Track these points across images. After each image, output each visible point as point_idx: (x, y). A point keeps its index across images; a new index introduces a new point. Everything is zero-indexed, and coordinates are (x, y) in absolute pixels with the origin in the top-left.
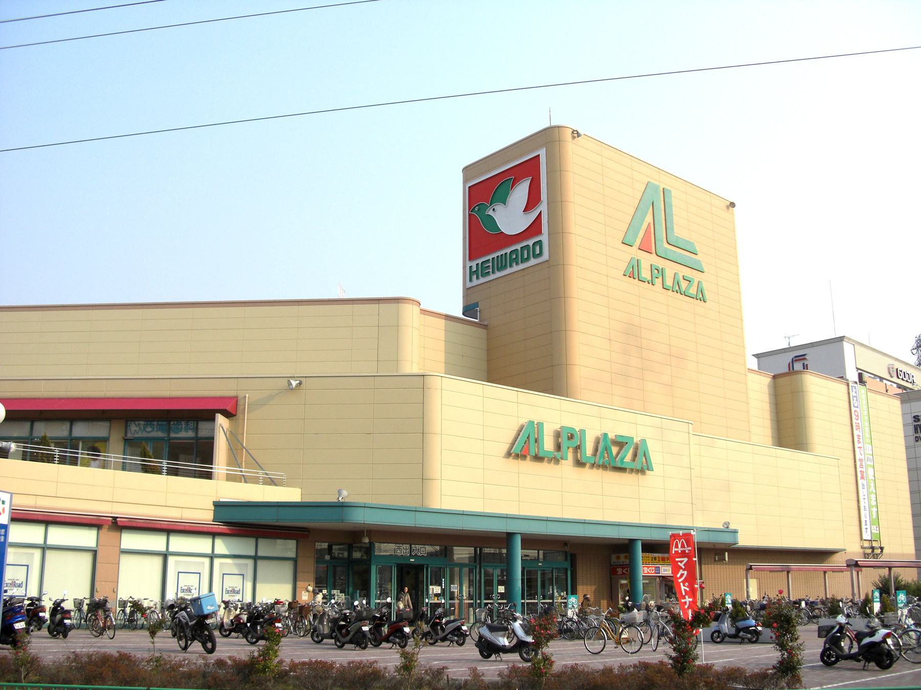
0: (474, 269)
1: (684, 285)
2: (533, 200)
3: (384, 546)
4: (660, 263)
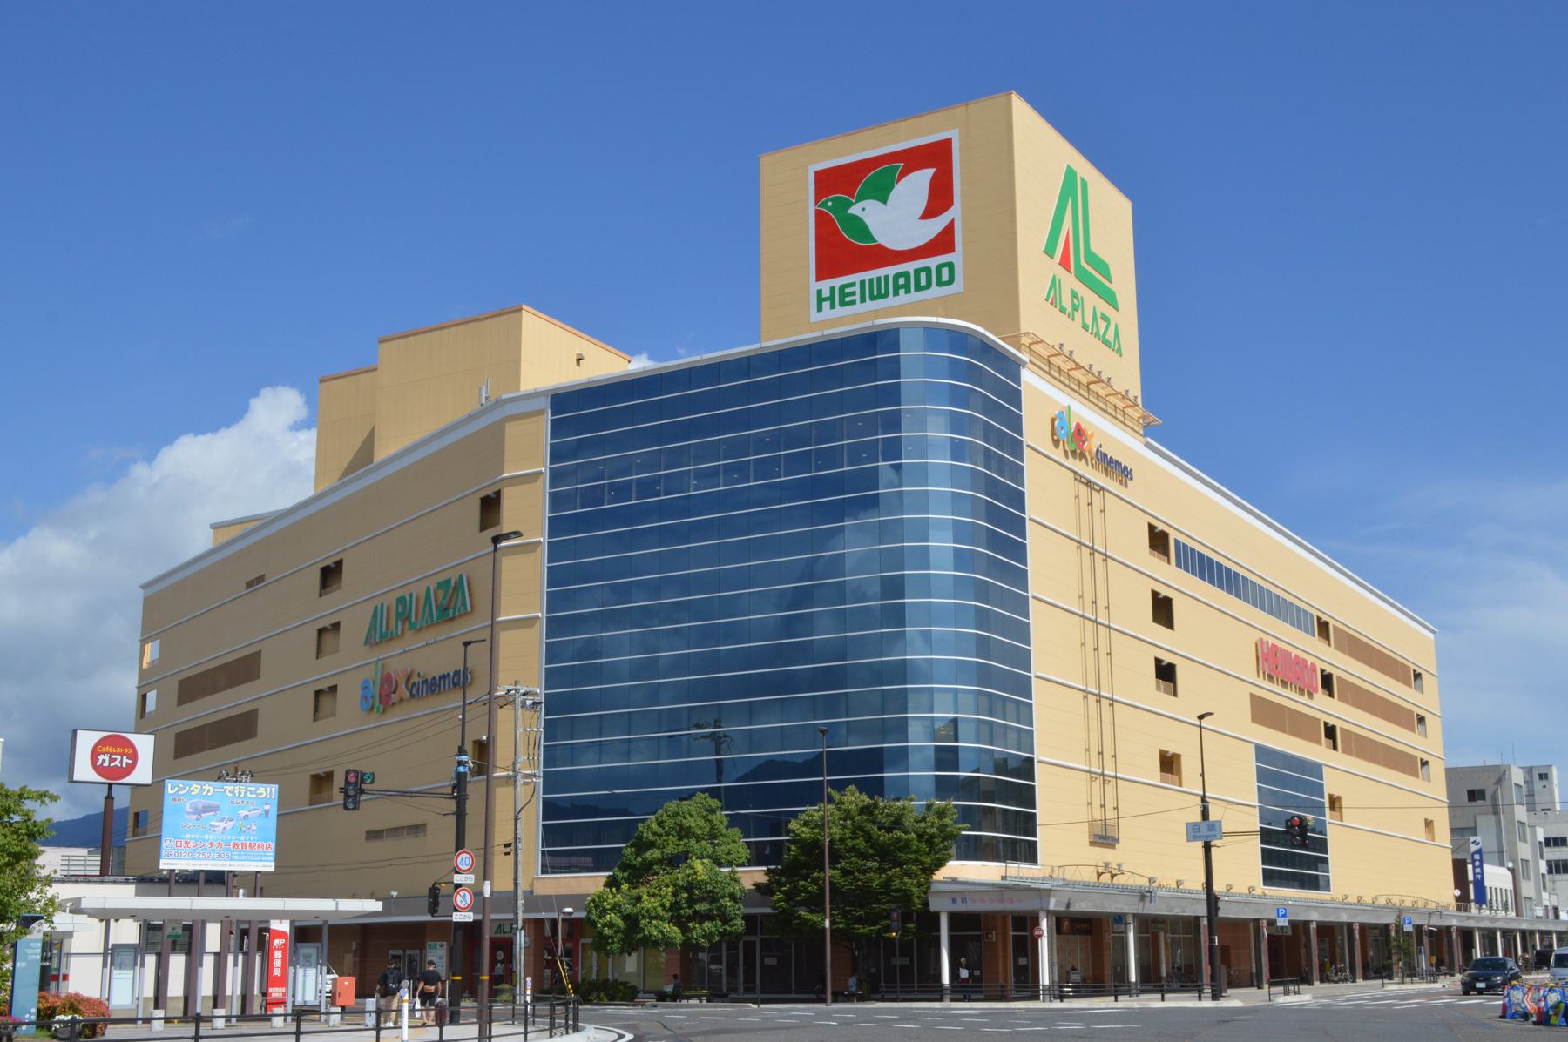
0: (826, 294)
1: (1103, 325)
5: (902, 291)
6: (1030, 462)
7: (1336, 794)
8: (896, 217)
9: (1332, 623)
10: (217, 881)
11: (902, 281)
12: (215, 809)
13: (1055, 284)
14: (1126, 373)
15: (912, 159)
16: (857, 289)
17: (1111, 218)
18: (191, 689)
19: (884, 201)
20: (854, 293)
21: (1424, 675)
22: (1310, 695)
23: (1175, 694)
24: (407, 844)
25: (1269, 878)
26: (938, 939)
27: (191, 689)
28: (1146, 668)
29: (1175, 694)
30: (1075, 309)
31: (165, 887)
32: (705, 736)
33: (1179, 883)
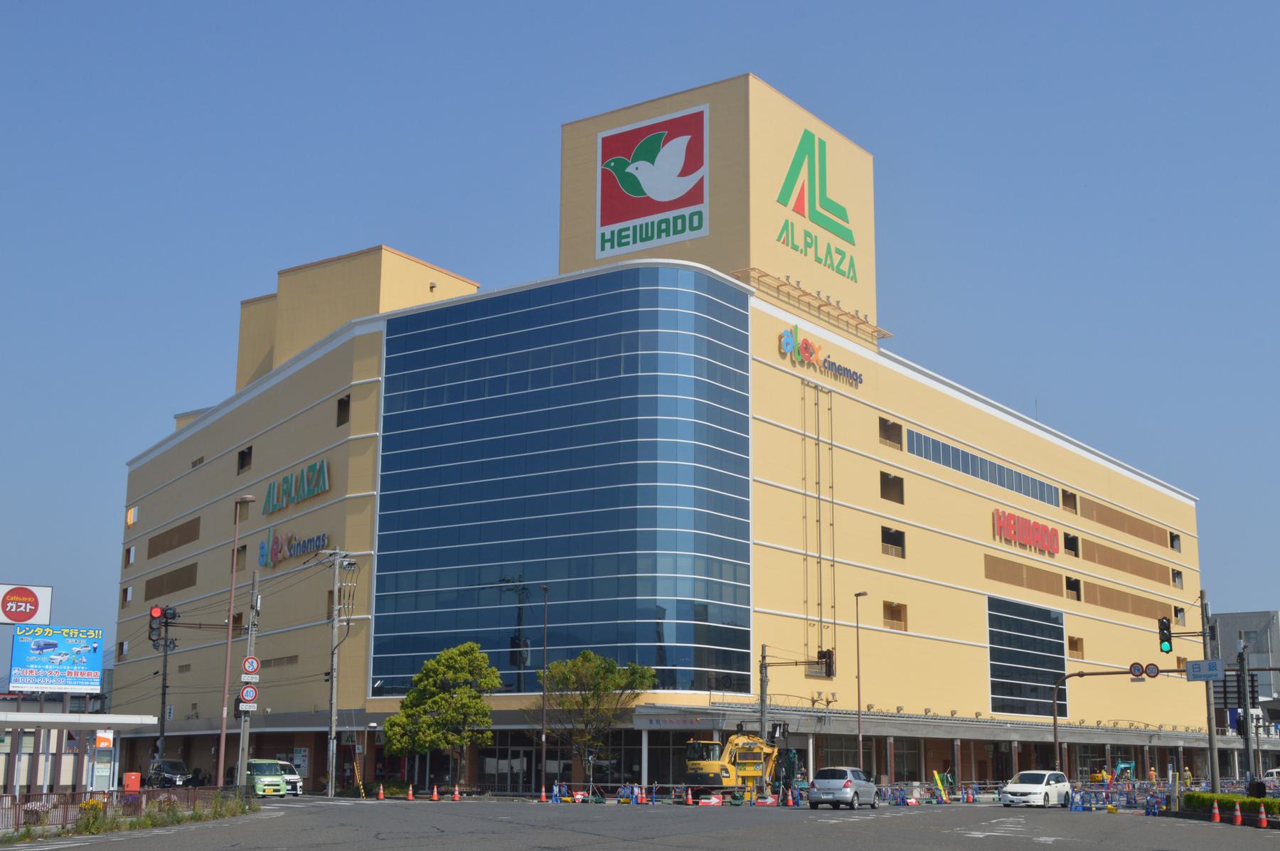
0: (608, 236)
1: (837, 258)
2: (693, 161)
3: (267, 779)
4: (815, 230)
5: (663, 235)
6: (754, 373)
7: (1076, 635)
8: (660, 176)
9: (1078, 495)
10: (55, 700)
11: (663, 226)
12: (54, 646)
13: (787, 227)
14: (861, 296)
15: (674, 128)
16: (630, 232)
17: (851, 173)
18: (158, 546)
19: (652, 162)
20: (628, 236)
21: (1182, 537)
22: (1051, 555)
23: (903, 557)
24: (288, 670)
25: (998, 706)
26: (640, 750)
27: (158, 546)
28: (854, 539)
29: (903, 557)
30: (808, 245)
31: (37, 705)
32: (510, 589)
33: (899, 709)
